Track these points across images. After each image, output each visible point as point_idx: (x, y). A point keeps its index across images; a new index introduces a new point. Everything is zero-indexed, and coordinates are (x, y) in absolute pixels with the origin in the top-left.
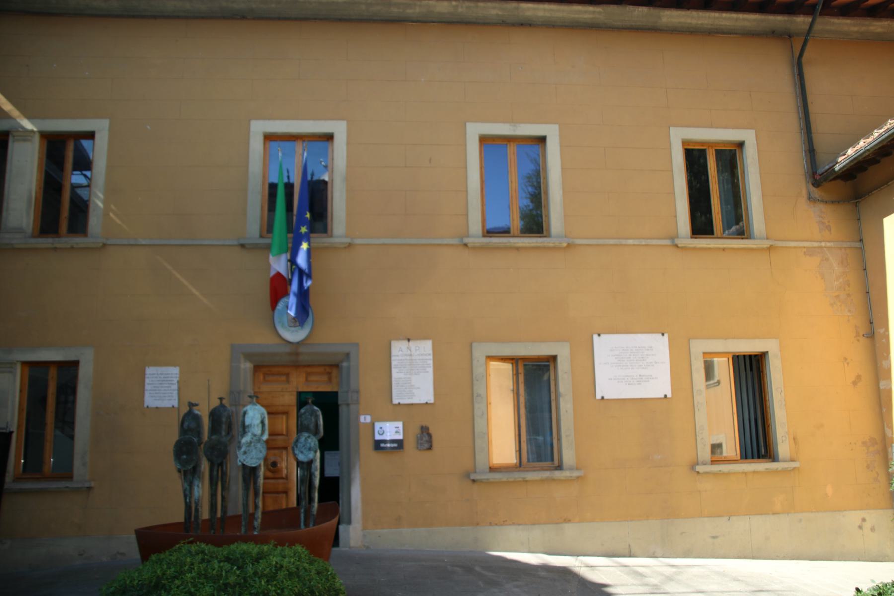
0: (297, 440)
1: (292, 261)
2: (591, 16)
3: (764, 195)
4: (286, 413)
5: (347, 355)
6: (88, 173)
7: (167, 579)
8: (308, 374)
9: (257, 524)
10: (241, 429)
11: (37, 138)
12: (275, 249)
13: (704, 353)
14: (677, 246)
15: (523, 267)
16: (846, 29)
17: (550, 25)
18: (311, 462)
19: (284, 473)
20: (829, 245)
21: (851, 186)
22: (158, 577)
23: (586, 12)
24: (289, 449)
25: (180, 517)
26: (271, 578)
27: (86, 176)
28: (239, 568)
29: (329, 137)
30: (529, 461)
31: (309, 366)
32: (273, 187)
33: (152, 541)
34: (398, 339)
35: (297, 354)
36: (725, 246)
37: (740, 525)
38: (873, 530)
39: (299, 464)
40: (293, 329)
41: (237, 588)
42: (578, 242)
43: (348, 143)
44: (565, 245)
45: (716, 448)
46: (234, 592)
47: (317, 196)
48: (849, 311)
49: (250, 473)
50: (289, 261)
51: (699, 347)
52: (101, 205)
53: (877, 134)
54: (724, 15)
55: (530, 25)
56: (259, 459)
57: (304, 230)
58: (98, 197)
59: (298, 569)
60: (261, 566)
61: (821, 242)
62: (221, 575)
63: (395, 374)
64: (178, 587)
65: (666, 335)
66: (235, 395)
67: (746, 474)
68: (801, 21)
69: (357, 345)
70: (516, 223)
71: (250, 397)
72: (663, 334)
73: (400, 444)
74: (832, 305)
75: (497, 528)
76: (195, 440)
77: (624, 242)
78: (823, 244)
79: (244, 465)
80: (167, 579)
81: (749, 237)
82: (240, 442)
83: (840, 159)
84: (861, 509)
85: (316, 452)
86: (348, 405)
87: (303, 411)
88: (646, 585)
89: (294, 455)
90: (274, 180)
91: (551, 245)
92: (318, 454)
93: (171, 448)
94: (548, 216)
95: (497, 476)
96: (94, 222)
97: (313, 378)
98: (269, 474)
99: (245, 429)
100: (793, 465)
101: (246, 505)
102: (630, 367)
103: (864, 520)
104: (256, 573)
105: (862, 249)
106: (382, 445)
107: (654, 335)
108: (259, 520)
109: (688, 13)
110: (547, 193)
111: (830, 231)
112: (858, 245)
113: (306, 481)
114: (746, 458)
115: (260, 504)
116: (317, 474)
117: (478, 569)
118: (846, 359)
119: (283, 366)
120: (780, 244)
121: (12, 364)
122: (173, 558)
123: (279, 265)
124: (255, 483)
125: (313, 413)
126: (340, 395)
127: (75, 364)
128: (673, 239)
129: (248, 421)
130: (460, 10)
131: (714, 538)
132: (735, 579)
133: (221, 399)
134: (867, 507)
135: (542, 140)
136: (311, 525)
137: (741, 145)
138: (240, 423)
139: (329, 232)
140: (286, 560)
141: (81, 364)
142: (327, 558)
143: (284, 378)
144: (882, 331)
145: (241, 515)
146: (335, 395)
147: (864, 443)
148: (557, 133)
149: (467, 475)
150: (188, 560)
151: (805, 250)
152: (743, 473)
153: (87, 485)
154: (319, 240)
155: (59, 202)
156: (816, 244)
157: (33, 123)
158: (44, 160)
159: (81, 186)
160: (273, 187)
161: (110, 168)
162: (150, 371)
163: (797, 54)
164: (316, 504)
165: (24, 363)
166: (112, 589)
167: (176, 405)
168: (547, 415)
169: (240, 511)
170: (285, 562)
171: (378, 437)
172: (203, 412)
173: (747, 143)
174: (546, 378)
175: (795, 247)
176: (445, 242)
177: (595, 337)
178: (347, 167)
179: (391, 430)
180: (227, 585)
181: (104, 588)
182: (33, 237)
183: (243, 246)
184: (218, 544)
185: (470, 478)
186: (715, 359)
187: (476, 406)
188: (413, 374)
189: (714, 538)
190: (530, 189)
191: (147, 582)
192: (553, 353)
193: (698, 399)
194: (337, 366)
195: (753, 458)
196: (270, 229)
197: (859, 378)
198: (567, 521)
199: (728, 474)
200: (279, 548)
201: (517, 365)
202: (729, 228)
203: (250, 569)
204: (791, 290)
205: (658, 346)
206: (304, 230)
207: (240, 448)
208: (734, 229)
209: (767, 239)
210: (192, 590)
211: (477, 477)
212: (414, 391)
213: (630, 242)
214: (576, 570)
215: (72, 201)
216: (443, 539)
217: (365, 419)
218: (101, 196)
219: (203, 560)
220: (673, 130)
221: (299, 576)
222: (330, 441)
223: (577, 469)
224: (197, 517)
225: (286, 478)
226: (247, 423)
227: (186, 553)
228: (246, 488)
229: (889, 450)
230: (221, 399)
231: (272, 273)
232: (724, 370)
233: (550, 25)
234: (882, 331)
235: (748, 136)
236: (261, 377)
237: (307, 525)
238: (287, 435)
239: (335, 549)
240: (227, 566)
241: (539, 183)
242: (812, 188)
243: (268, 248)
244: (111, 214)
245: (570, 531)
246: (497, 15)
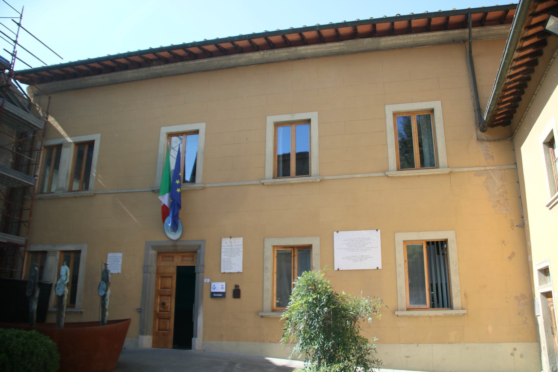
2: (338, 48)
8: (183, 257)
11: (73, 146)
14: (387, 176)
16: (503, 32)
17: (316, 56)
20: (492, 168)
23: (335, 46)
34: (225, 237)
35: (176, 246)
36: (419, 174)
43: (206, 134)
44: (319, 180)
48: (507, 210)
52: (94, 175)
54: (420, 35)
61: (486, 167)
63: (223, 257)
65: (379, 231)
67: (430, 317)
69: (205, 240)
72: (377, 230)
73: (224, 295)
74: (494, 207)
75: (274, 344)
77: (354, 176)
78: (488, 168)
84: (513, 342)
91: (311, 181)
97: (185, 259)
98: (162, 309)
103: (515, 349)
106: (214, 295)
107: (371, 231)
109: (397, 37)
111: (493, 159)
112: (513, 167)
114: (433, 307)
118: (504, 242)
119: (171, 253)
120: (457, 170)
121: (55, 252)
130: (266, 56)
134: (519, 341)
137: (432, 111)
143: (171, 259)
146: (193, 268)
147: (516, 298)
148: (317, 116)
149: (257, 313)
151: (475, 172)
152: (428, 316)
153: (80, 310)
156: (482, 168)
162: (110, 255)
167: (120, 272)
171: (213, 291)
176: (252, 183)
177: (335, 233)
178: (205, 146)
179: (219, 287)
183: (153, 191)
187: (265, 274)
188: (232, 256)
189: (407, 357)
192: (310, 243)
197: (513, 254)
199: (418, 317)
205: (374, 238)
213: (358, 176)
217: (207, 280)
220: (439, 102)
233: (316, 56)
235: (436, 105)
238: (171, 288)
242: (479, 132)
244: (99, 180)
246: (286, 56)
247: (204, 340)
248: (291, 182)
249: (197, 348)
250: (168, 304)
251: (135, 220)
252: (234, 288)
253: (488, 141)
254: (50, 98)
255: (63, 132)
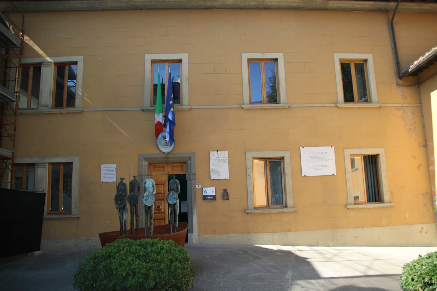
0: (169, 195)
1: (166, 117)
2: (297, 4)
3: (377, 84)
4: (163, 184)
5: (190, 158)
6: (75, 81)
7: (113, 253)
8: (173, 167)
9: (152, 231)
10: (144, 190)
11: (53, 65)
12: (157, 111)
13: (351, 155)
14: (338, 107)
15: (269, 120)
18: (175, 204)
19: (163, 210)
20: (406, 105)
21: (417, 79)
22: (109, 252)
24: (165, 200)
25: (118, 229)
26: (158, 253)
27: (73, 82)
28: (144, 249)
29: (180, 61)
30: (272, 204)
31: (173, 163)
32: (156, 86)
33: (106, 238)
34: (212, 151)
35: (168, 158)
37: (367, 232)
38: (426, 233)
39: (169, 205)
40: (166, 147)
41: (144, 257)
42: (293, 106)
43: (189, 64)
44: (287, 107)
45: (356, 198)
46: (143, 259)
47: (175, 89)
49: (148, 209)
50: (163, 116)
51: (348, 152)
52: (80, 94)
53: (428, 54)
54: (357, 2)
55: (270, 9)
56: (152, 203)
57: (171, 102)
58: (79, 90)
59: (170, 249)
60: (154, 248)
62: (137, 252)
64: (118, 257)
65: (333, 147)
66: (141, 176)
67: (370, 209)
68: (392, 4)
70: (265, 99)
71: (147, 175)
73: (214, 197)
75: (258, 234)
76: (124, 194)
77: (314, 105)
78: (404, 105)
79: (145, 206)
80: (113, 253)
81: (370, 102)
82: (143, 195)
83: (411, 66)
84: (421, 224)
85: (177, 200)
86: (191, 180)
87: (171, 181)
88: (325, 258)
89: (167, 201)
90: (156, 82)
91: (281, 107)
92: (178, 201)
93: (114, 201)
94: (279, 94)
95: (258, 211)
96: (78, 101)
97: (175, 169)
98: (156, 211)
99: (145, 189)
100: (391, 204)
101: (147, 223)
102: (317, 162)
103: (422, 228)
104: (152, 251)
105: (421, 107)
106: (206, 198)
108: (153, 230)
110: (278, 84)
112: (419, 105)
113: (173, 213)
114: (370, 202)
115: (153, 222)
116: (178, 209)
117: (250, 252)
118: (414, 157)
120: (384, 105)
121: (44, 164)
122: (116, 244)
123: (159, 118)
124: (151, 213)
125: (175, 182)
126: (187, 176)
127: (71, 164)
128: (336, 103)
129: (147, 186)
130: (238, 3)
131: (355, 237)
132: (365, 255)
133: (134, 177)
135: (276, 60)
136: (176, 231)
137: (366, 61)
138: (143, 187)
139: (181, 103)
140: (165, 245)
141: (73, 164)
142: (183, 246)
143: (162, 169)
144: (430, 144)
145: (144, 228)
146: (185, 176)
147: (423, 194)
148: (283, 57)
150: (122, 245)
153: (78, 216)
154: (177, 107)
155: (62, 93)
156: (400, 105)
157: (51, 59)
158: (56, 75)
159: (72, 87)
160: (156, 86)
161: (84, 77)
162: (103, 166)
163: (391, 19)
164: (178, 223)
165: (50, 164)
166: (90, 257)
168: (280, 185)
169: (144, 226)
170: (165, 246)
171: (204, 194)
172: (127, 182)
173: (369, 60)
174: (279, 169)
175: (391, 107)
177: (301, 148)
178: (189, 74)
179: (210, 191)
180: (139, 256)
181: (87, 257)
182: (52, 108)
184: (135, 239)
185: (246, 212)
186: (355, 158)
187: (248, 180)
188: (220, 166)
189: (355, 237)
190: (271, 84)
191: (105, 254)
193: (348, 175)
194: (186, 163)
195: (373, 202)
196: (155, 103)
198: (289, 231)
199: (361, 209)
200: (162, 241)
201: (266, 162)
202: (361, 99)
203: (149, 249)
204: (389, 124)
206: (171, 102)
207: (143, 198)
208: (363, 99)
209: (379, 103)
210: (124, 258)
211: (250, 212)
212: (220, 173)
213: (316, 105)
214: (294, 252)
215: (68, 93)
216: (234, 239)
217: (198, 186)
218: (81, 90)
219: (128, 245)
220: (335, 54)
221: (171, 253)
222: (183, 196)
223: (391, 203)
224: (125, 228)
225: (164, 213)
226: (146, 187)
227: (120, 242)
228: (147, 216)
229: (434, 197)
230: (134, 177)
231: (156, 122)
232: (360, 163)
234: (430, 144)
235: (369, 57)
236: (152, 168)
237: (173, 232)
238: (164, 194)
239: (186, 244)
240: (139, 248)
241: (275, 81)
242: (399, 80)
243: (154, 111)
244: (85, 98)
245: (291, 235)
247: (199, 235)
248: (266, 108)
249: (194, 241)
250: (162, 207)
251: (126, 135)
252: (222, 191)
253: (404, 86)
254: (24, 17)
255: (41, 52)
